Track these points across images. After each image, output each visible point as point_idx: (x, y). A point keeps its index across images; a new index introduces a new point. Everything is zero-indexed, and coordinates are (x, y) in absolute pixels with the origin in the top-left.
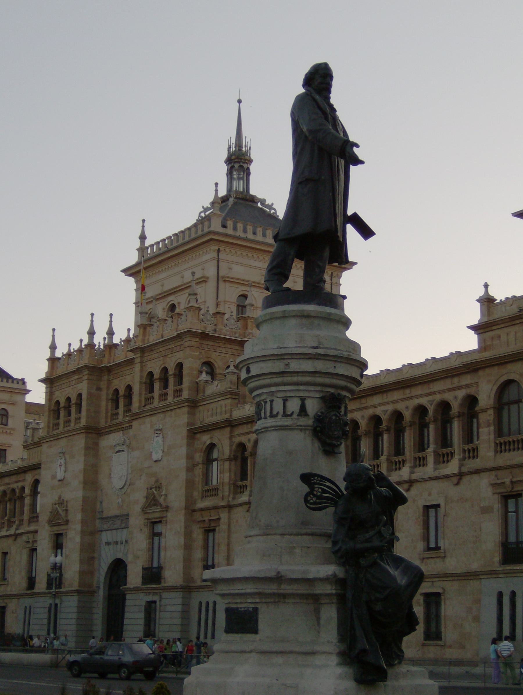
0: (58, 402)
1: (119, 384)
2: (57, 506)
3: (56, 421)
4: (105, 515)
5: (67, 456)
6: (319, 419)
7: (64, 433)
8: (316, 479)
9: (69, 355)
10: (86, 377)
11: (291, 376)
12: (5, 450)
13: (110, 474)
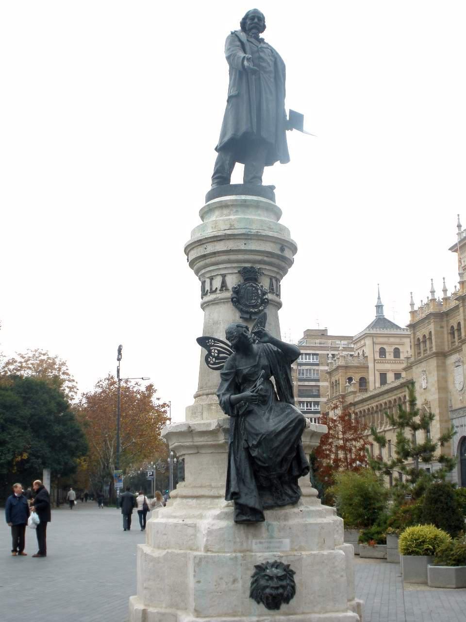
0: (419, 339)
1: (453, 323)
2: (424, 405)
3: (419, 351)
4: (454, 408)
5: (427, 373)
6: (236, 291)
7: (423, 359)
8: (212, 342)
9: (421, 308)
10: (432, 321)
11: (211, 258)
12: (386, 374)
13: (454, 382)
